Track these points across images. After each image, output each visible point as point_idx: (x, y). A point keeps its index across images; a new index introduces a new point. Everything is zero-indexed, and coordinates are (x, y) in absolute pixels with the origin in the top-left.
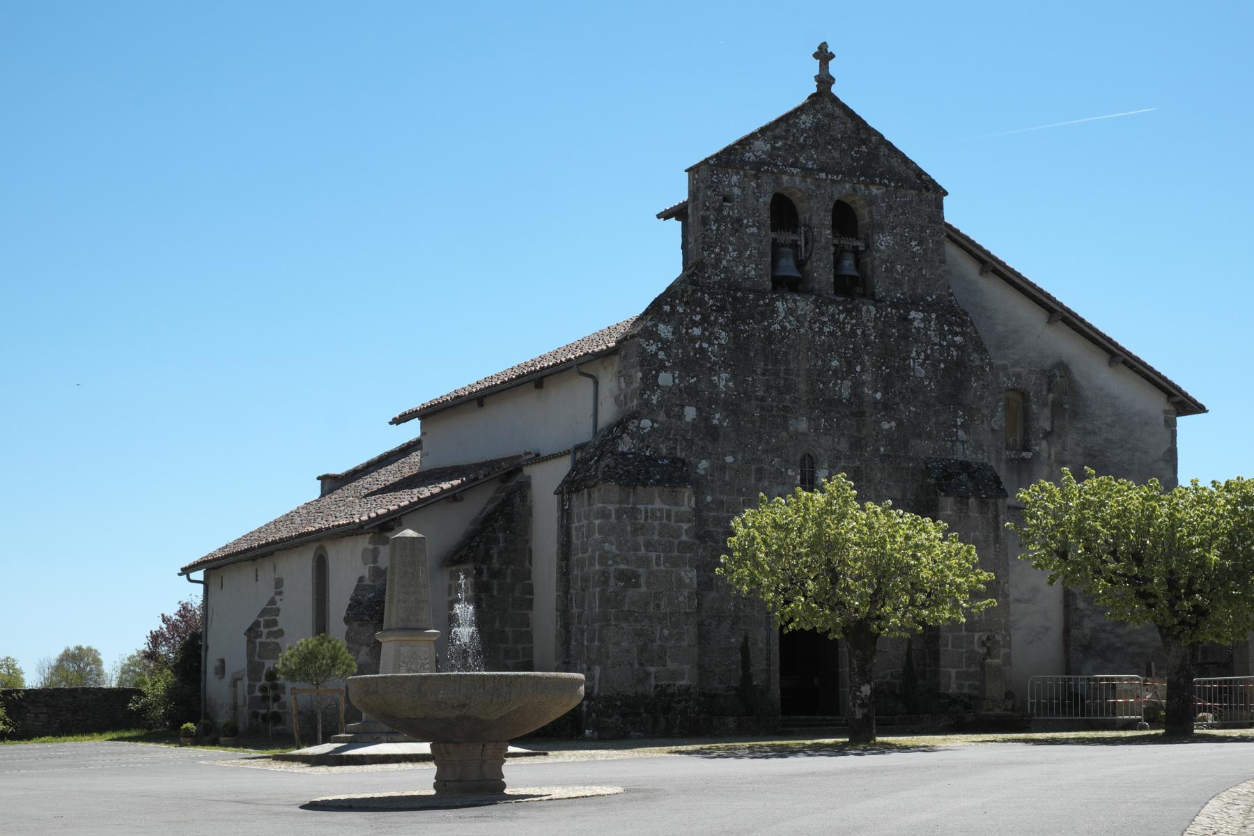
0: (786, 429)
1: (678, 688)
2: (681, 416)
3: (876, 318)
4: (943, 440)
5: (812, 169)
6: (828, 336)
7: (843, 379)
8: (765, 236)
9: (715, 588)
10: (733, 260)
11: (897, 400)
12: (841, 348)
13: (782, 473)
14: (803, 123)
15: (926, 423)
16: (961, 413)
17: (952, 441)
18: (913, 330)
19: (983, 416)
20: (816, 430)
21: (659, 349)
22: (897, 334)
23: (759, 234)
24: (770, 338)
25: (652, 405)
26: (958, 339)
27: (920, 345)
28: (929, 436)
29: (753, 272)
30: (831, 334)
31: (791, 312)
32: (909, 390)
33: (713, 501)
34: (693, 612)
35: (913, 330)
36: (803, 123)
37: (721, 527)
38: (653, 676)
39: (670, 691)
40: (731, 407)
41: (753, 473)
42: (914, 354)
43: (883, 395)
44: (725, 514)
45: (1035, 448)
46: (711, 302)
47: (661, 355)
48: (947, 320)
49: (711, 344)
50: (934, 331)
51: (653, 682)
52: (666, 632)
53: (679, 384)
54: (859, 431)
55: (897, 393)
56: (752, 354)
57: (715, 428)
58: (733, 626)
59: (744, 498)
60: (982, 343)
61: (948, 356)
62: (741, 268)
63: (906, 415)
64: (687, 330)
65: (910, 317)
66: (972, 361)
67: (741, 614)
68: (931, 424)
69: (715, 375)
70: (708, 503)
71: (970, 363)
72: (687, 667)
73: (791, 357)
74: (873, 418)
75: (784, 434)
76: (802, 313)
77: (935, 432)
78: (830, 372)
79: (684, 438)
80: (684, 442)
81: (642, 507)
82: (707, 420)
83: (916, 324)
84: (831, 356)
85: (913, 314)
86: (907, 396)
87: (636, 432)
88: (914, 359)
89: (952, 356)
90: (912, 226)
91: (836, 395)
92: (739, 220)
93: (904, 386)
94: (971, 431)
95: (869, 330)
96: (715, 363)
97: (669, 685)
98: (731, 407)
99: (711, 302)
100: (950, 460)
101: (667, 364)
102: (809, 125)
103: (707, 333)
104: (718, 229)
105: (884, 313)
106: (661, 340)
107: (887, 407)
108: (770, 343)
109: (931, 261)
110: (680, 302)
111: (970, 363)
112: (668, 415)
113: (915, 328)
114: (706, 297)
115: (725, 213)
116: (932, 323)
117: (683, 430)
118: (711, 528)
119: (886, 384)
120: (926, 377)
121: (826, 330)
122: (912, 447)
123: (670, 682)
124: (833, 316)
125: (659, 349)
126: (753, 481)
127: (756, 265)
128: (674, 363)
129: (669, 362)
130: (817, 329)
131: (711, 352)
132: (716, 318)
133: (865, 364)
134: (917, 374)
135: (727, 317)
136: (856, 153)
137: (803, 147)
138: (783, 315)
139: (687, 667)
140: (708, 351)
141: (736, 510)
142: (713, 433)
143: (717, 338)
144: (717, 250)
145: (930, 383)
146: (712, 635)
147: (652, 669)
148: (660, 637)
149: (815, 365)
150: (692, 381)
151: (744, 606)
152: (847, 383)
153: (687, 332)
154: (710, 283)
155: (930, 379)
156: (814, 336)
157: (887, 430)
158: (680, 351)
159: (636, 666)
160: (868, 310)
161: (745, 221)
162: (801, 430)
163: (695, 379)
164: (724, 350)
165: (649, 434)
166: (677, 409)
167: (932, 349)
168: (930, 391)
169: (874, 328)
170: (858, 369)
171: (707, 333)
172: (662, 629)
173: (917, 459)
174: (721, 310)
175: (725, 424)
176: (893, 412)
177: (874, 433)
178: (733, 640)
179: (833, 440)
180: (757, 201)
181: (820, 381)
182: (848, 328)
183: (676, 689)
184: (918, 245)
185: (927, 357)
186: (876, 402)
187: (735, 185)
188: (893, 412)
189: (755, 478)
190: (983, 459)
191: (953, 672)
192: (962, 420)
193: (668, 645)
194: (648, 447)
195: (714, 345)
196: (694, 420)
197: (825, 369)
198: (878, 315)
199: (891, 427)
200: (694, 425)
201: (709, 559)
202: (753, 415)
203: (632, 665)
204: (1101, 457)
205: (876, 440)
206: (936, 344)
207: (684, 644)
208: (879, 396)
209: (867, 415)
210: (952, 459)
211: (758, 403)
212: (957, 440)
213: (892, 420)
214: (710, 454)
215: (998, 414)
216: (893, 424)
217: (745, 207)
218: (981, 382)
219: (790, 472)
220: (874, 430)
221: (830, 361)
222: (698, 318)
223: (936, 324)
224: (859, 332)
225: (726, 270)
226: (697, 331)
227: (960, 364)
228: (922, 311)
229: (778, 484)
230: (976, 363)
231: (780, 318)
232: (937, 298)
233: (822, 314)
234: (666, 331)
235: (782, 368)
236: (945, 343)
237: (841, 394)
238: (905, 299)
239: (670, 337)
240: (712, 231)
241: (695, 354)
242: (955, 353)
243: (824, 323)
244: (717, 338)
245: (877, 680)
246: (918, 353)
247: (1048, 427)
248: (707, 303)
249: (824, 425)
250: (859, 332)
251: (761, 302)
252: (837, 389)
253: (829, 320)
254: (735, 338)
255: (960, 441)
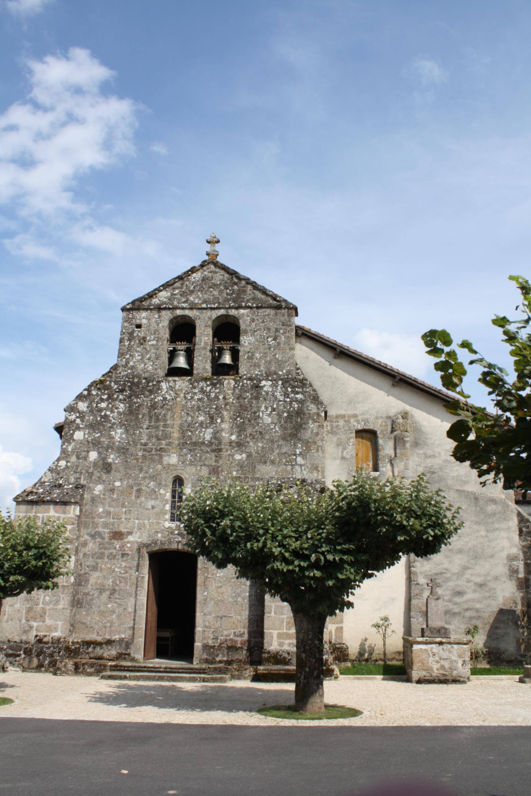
0: (160, 462)
1: (52, 638)
2: (86, 458)
3: (234, 387)
4: (285, 465)
5: (198, 303)
6: (197, 402)
7: (207, 427)
8: (161, 345)
9: (99, 570)
10: (138, 361)
11: (248, 439)
12: (206, 408)
13: (155, 492)
14: (194, 278)
15: (271, 454)
16: (300, 446)
17: (292, 465)
18: (263, 393)
19: (318, 447)
20: (183, 462)
21: (77, 417)
22: (250, 397)
23: (157, 345)
24: (154, 406)
25: (68, 451)
26: (299, 396)
27: (268, 402)
28: (273, 462)
29: (151, 367)
30: (199, 400)
31: (171, 388)
32: (258, 433)
33: (103, 512)
34: (69, 586)
35: (263, 393)
36: (194, 278)
37: (108, 528)
38: (34, 629)
39: (45, 640)
40: (122, 451)
41: (134, 492)
42: (263, 408)
43: (238, 437)
44: (111, 520)
45: (382, 469)
46: (116, 387)
47: (78, 421)
48: (290, 384)
49: (112, 412)
50: (280, 392)
51: (35, 633)
52: (47, 598)
53: (87, 438)
54: (216, 461)
55: (248, 435)
56: (140, 416)
57: (110, 465)
58: (111, 596)
59: (126, 509)
60: (318, 398)
61: (290, 408)
62: (143, 365)
63: (254, 450)
64: (97, 404)
65: (261, 385)
66: (309, 410)
67: (117, 588)
68: (275, 454)
69: (113, 431)
70: (100, 513)
71: (309, 412)
72: (60, 623)
73: (168, 417)
74: (229, 452)
75: (159, 467)
76: (180, 388)
77: (278, 460)
78: (197, 424)
79: (87, 471)
80: (87, 474)
81: (40, 515)
82: (104, 459)
83: (265, 389)
84: (199, 414)
85: (263, 383)
86: (256, 437)
87: (55, 469)
88: (263, 412)
89: (294, 408)
90: (269, 329)
91: (200, 439)
92: (144, 339)
93: (254, 430)
94: (308, 457)
95: (229, 395)
96: (114, 424)
97: (45, 636)
98: (122, 451)
99: (116, 387)
100: (289, 478)
101: (81, 426)
102: (198, 279)
103: (110, 406)
104: (129, 344)
105: (241, 384)
106: (79, 412)
107: (240, 445)
108: (155, 409)
109: (283, 349)
110: (95, 388)
111: (309, 412)
112: (78, 458)
113: (265, 391)
114: (113, 384)
115: (135, 335)
116: (279, 388)
117: (87, 466)
118: (100, 529)
119: (241, 429)
120: (272, 423)
121: (196, 397)
122: (259, 471)
123: (46, 634)
124: (202, 388)
125: (77, 417)
126: (134, 498)
127: (153, 363)
128: (86, 426)
129: (83, 424)
130: (189, 398)
131: (112, 417)
132: (118, 396)
133: (224, 418)
134: (265, 422)
135: (126, 395)
136: (230, 290)
137: (192, 292)
138: (166, 390)
139: (60, 623)
140: (110, 416)
141: (120, 517)
142: (107, 468)
143: (117, 408)
144: (128, 356)
145: (275, 427)
146: (94, 601)
147: (35, 624)
148: (43, 602)
149: (186, 421)
150: (97, 435)
151: (120, 582)
152: (210, 430)
153: (97, 407)
154: (120, 376)
155: (275, 424)
156: (186, 402)
157: (239, 460)
158: (91, 417)
159: (24, 621)
160: (229, 383)
161: (148, 338)
162: (171, 463)
163: (99, 434)
164: (121, 415)
165: (64, 470)
166: (85, 453)
167: (278, 404)
168: (275, 432)
169: (232, 394)
170: (219, 421)
171: (110, 406)
172: (45, 596)
173: (262, 479)
174: (122, 391)
175: (117, 462)
176: (244, 448)
177: (228, 462)
178: (109, 606)
179: (196, 469)
180: (158, 325)
181: (189, 430)
182: (213, 395)
183: (50, 638)
184: (274, 340)
185: (274, 410)
186: (231, 442)
187: (144, 318)
188: (244, 448)
189: (135, 496)
190: (318, 476)
191: (275, 633)
192: (301, 450)
193: (47, 608)
194: (61, 478)
195: (114, 412)
196: (95, 460)
197: (194, 422)
198: (236, 385)
199: (242, 458)
200: (95, 464)
201: (97, 550)
202: (138, 455)
203: (20, 621)
204: (440, 473)
205: (230, 467)
206: (281, 401)
207: (60, 606)
208: (234, 437)
209: (224, 450)
210: (292, 477)
211: (142, 447)
212: (296, 464)
213: (243, 453)
214: (104, 481)
215: (350, 447)
216: (244, 455)
217: (149, 330)
218: (317, 424)
219: (162, 491)
220: (229, 460)
221: (198, 417)
222: (105, 397)
223: (281, 388)
224: (221, 397)
225: (132, 367)
226: (103, 405)
227: (299, 413)
228: (271, 381)
229: (152, 499)
230: (313, 411)
231: (163, 393)
232: (287, 372)
233: (194, 388)
234: (83, 406)
235: (162, 424)
236: (288, 400)
237: (204, 438)
238: (262, 375)
239: (85, 409)
240: (125, 345)
241: (101, 419)
242: (296, 406)
243: (195, 394)
244: (117, 408)
245: (222, 638)
246: (266, 408)
247: (392, 453)
248: (112, 387)
249: (190, 459)
250: (221, 397)
251: (151, 384)
252: (201, 435)
253: (199, 391)
254: (130, 407)
255: (299, 465)
